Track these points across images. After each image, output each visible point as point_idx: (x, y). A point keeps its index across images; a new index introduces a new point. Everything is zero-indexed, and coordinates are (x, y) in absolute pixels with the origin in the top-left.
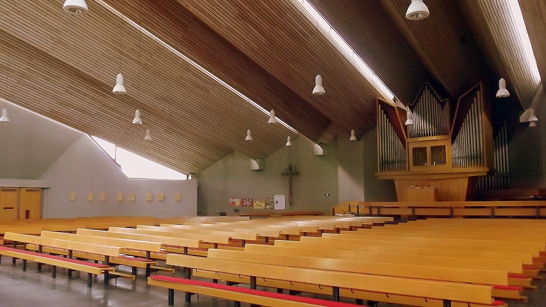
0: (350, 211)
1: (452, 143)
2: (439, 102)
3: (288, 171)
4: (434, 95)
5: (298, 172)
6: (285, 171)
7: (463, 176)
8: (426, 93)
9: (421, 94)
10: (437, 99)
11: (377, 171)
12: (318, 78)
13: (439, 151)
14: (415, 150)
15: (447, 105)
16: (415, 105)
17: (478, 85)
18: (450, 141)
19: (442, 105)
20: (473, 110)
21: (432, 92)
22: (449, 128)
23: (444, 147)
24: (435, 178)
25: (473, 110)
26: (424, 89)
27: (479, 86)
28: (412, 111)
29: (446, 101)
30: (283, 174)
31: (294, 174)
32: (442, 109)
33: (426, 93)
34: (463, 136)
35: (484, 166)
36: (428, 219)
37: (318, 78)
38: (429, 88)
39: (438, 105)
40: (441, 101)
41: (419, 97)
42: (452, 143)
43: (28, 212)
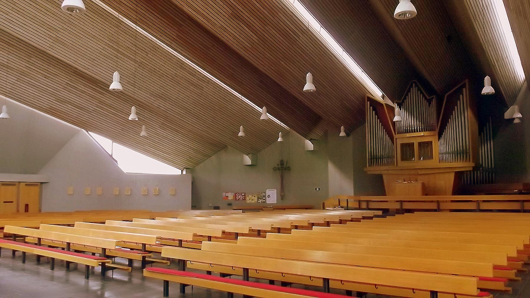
0: (339, 205)
1: (439, 139)
2: (426, 99)
3: (280, 166)
4: (421, 92)
5: (289, 167)
6: (277, 166)
7: (450, 170)
8: (414, 90)
9: (409, 91)
10: (424, 96)
12: (309, 76)
13: (426, 146)
15: (434, 102)
16: (403, 102)
17: (464, 82)
18: (437, 137)
19: (429, 102)
20: (459, 107)
21: (419, 89)
22: (435, 124)
23: (431, 142)
25: (459, 107)
26: (411, 86)
27: (465, 83)
29: (433, 98)
30: (275, 169)
31: (285, 169)
32: (429, 106)
33: (414, 90)
34: (449, 132)
35: (469, 161)
37: (309, 76)
39: (425, 102)
40: (428, 98)
42: (439, 139)
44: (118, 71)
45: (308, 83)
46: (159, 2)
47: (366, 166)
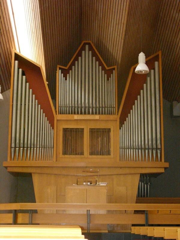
0: (147, 214)
1: (121, 126)
2: (103, 68)
4: (97, 59)
7: (133, 171)
9: (80, 54)
10: (100, 64)
11: (7, 160)
12: (142, 57)
13: (101, 135)
14: (65, 130)
16: (70, 68)
17: (157, 54)
19: (109, 73)
20: (112, 78)
21: (94, 54)
22: (114, 103)
23: (109, 130)
25: (112, 78)
26: (83, 48)
27: (158, 55)
28: (65, 76)
29: (114, 69)
32: (108, 79)
34: (134, 115)
35: (161, 160)
37: (142, 57)
38: (91, 49)
39: (102, 73)
40: (107, 68)
41: (76, 59)
42: (121, 126)
44: (105, 71)
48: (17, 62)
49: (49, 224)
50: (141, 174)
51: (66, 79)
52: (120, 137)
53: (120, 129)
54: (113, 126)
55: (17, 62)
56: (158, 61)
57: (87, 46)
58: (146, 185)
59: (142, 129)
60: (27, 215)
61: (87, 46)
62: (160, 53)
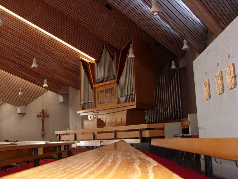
3: (41, 114)
4: (109, 52)
5: (48, 114)
6: (39, 114)
7: (121, 109)
8: (105, 50)
9: (102, 51)
10: (110, 54)
15: (115, 58)
18: (116, 84)
19: (113, 57)
21: (107, 50)
24: (207, 7)
26: (103, 48)
27: (131, 41)
29: (115, 54)
30: (38, 116)
31: (45, 116)
33: (105, 50)
34: (123, 78)
36: (119, 108)
38: (106, 47)
43: (218, 65)
44: (174, 61)
45: (130, 53)
46: (58, 2)
47: (181, 119)
48: (81, 63)
49: (127, 131)
50: (127, 110)
51: (98, 66)
52: (81, 96)
53: (117, 86)
54: (114, 85)
55: (81, 63)
56: (132, 43)
57: (105, 46)
58: (166, 106)
59: (128, 83)
60: (232, 87)
61: (105, 46)
62: (115, 53)
